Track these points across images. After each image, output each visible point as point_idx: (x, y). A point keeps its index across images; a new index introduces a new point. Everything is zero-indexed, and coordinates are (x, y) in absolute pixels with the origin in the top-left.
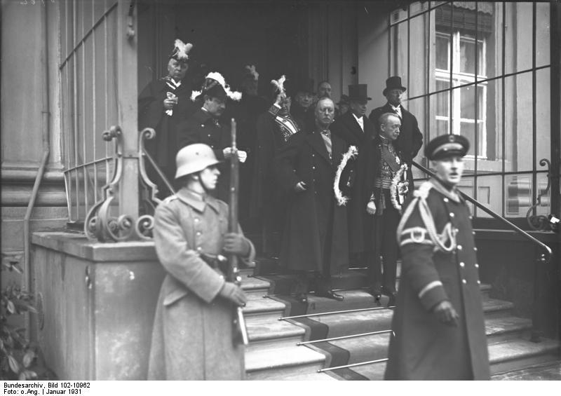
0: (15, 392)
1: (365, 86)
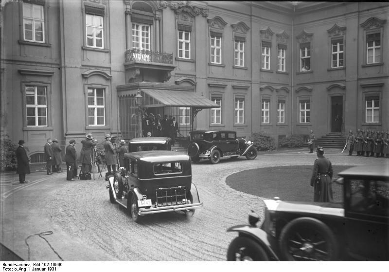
0: (10, 269)
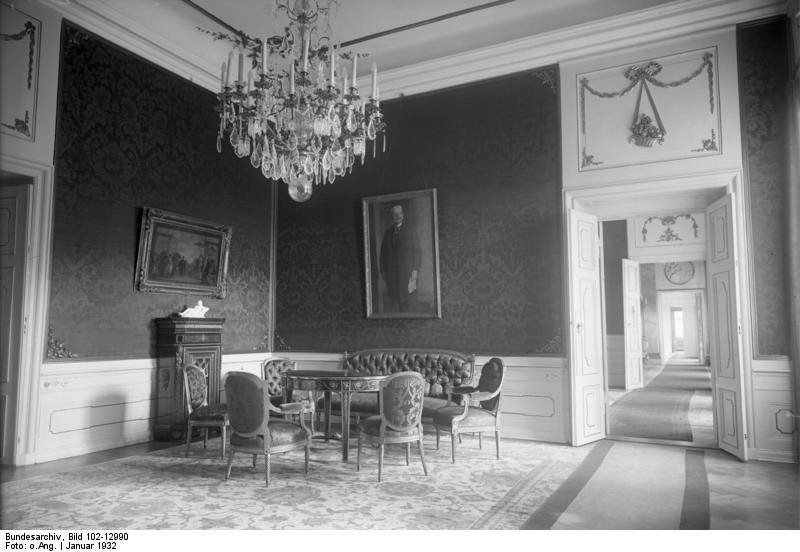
0: (21, 547)
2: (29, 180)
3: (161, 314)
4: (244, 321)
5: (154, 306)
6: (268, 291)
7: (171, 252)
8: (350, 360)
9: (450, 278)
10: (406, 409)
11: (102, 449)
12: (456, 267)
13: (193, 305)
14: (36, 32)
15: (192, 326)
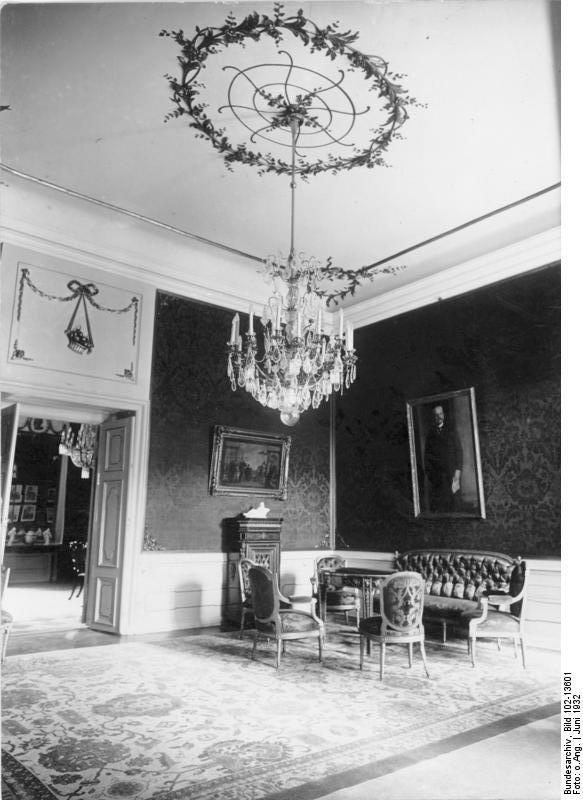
1: (297, 36)
2: (133, 413)
3: (231, 515)
4: (305, 521)
5: (224, 508)
6: (329, 492)
7: (239, 461)
8: (400, 559)
9: (493, 477)
10: (406, 608)
11: (183, 628)
12: (498, 465)
13: (256, 506)
14: (139, 303)
15: (254, 525)
